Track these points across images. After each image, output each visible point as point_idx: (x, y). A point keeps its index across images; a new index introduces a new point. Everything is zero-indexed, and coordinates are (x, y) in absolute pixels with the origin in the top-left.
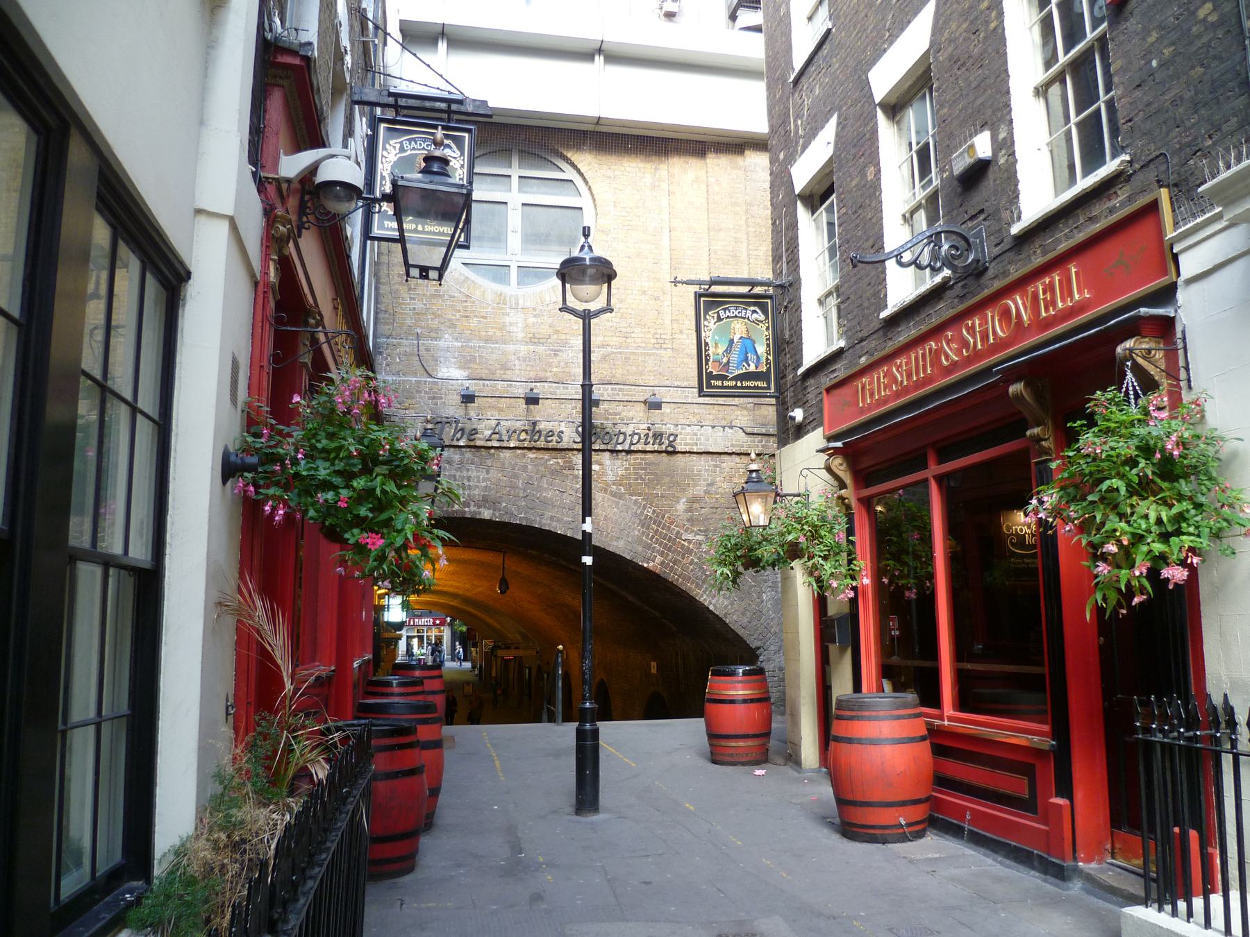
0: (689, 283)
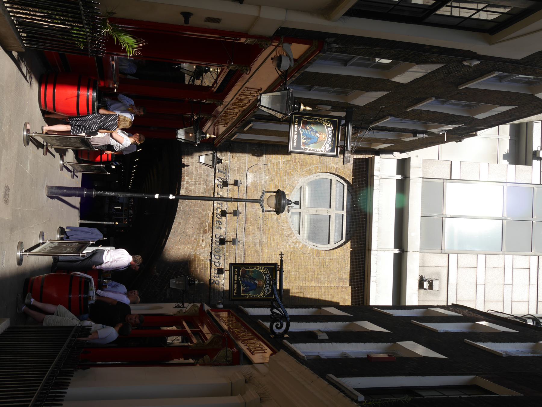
0: (282, 261)
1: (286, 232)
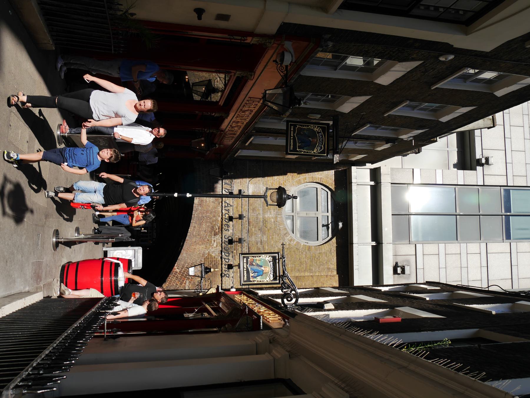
1: (283, 232)
